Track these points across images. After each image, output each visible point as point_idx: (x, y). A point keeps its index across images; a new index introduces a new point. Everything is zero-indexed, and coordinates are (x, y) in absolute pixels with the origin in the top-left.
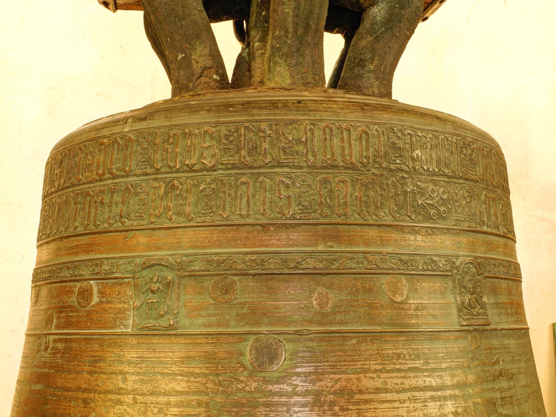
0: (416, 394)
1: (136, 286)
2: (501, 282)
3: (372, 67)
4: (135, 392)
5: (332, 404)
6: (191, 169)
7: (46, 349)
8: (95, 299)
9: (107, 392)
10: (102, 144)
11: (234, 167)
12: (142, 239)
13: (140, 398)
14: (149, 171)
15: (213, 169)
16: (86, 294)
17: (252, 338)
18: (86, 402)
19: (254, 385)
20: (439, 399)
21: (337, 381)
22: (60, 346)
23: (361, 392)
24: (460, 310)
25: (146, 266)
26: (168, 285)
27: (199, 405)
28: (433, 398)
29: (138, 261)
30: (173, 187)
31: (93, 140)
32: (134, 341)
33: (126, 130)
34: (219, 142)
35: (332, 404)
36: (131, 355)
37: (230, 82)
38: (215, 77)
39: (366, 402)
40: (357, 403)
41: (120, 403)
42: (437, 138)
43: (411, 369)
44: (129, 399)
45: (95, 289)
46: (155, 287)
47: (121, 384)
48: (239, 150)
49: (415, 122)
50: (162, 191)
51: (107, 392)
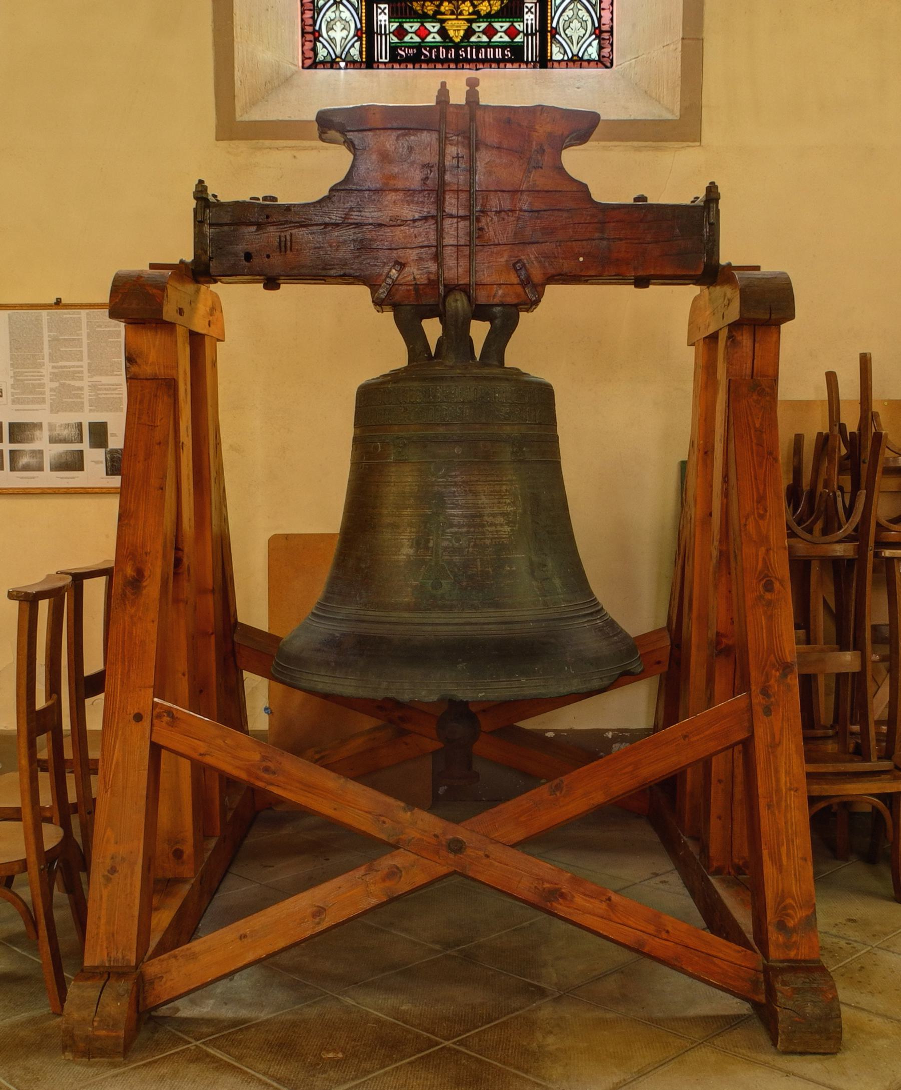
0: (491, 483)
1: (394, 445)
2: (111, 434)
3: (494, 348)
4: (395, 482)
5: (460, 486)
6: (413, 403)
7: (362, 468)
8: (380, 450)
9: (385, 482)
10: (380, 391)
11: (428, 403)
12: (396, 428)
13: (396, 484)
14: (398, 403)
15: (420, 403)
16: (376, 448)
17: (434, 464)
18: (378, 486)
19: (434, 479)
20: (499, 485)
21: (462, 478)
22: (367, 467)
23: (470, 482)
24: (511, 454)
25: (398, 438)
26: (405, 445)
27: (416, 485)
28: (497, 485)
29: (395, 436)
30: (407, 410)
31: (376, 389)
32: (394, 464)
33: (390, 386)
34: (423, 394)
35: (460, 486)
36: (393, 469)
37: (433, 355)
38: (426, 355)
39: (472, 485)
40: (469, 485)
41: (390, 486)
42: (505, 388)
43: (490, 474)
44: (393, 484)
45: (380, 446)
46: (401, 445)
47: (390, 480)
48: (430, 396)
49: (669, 271)
50: (403, 411)
51: (385, 482)
